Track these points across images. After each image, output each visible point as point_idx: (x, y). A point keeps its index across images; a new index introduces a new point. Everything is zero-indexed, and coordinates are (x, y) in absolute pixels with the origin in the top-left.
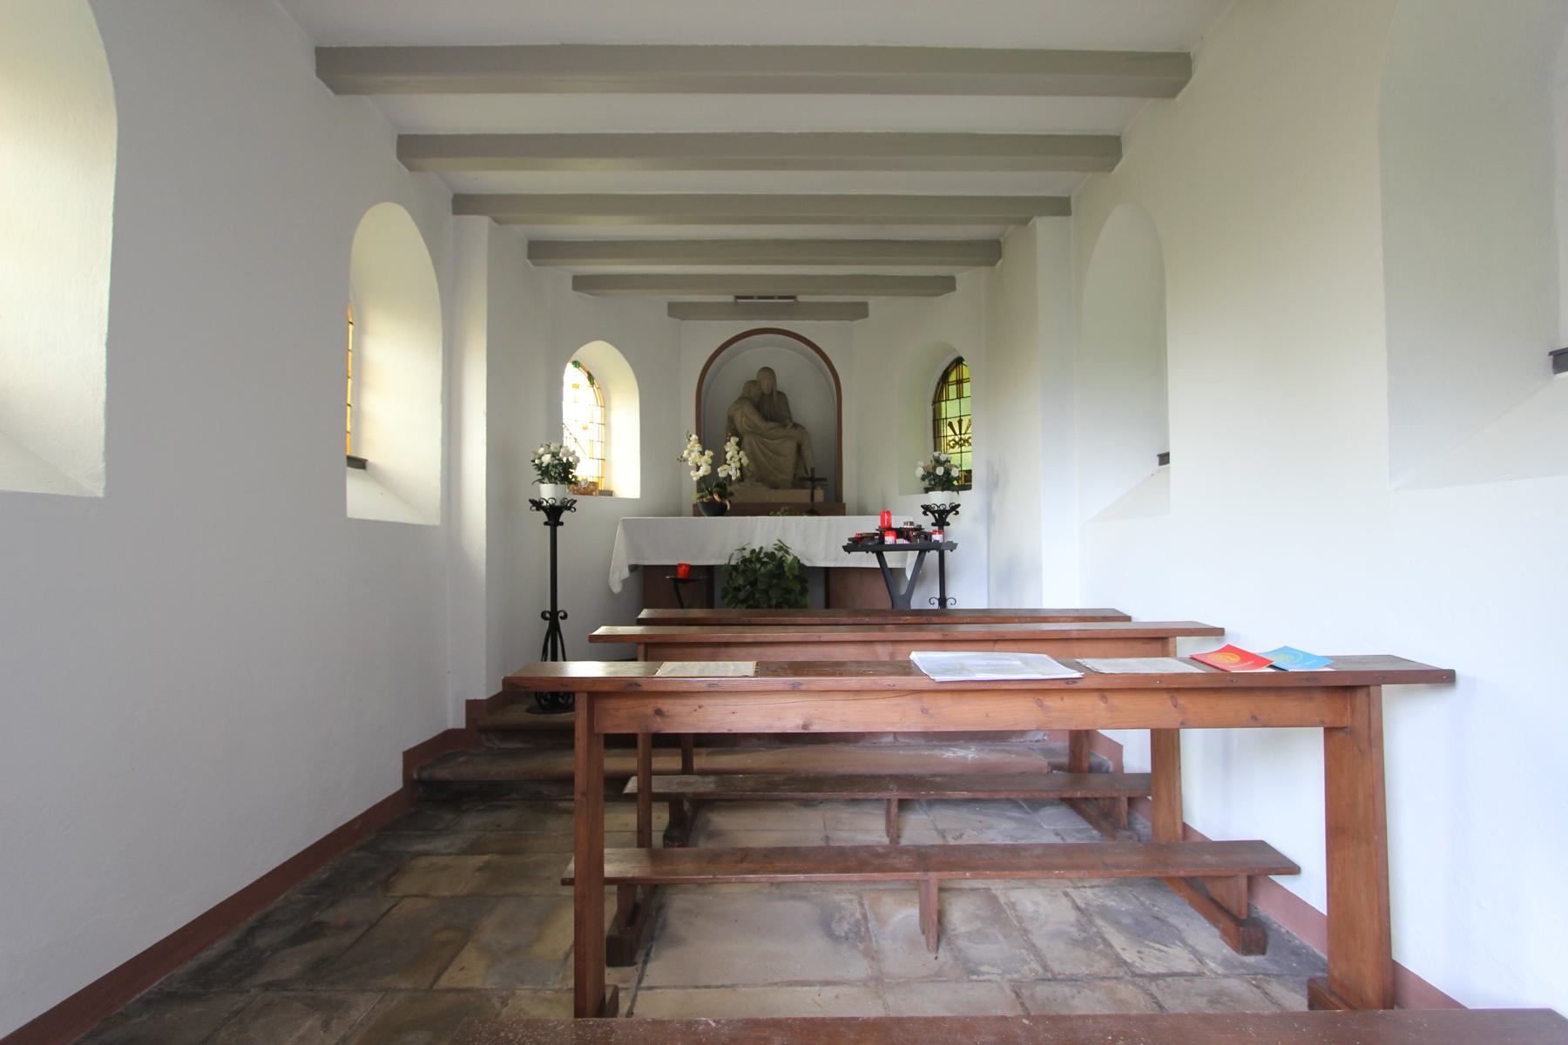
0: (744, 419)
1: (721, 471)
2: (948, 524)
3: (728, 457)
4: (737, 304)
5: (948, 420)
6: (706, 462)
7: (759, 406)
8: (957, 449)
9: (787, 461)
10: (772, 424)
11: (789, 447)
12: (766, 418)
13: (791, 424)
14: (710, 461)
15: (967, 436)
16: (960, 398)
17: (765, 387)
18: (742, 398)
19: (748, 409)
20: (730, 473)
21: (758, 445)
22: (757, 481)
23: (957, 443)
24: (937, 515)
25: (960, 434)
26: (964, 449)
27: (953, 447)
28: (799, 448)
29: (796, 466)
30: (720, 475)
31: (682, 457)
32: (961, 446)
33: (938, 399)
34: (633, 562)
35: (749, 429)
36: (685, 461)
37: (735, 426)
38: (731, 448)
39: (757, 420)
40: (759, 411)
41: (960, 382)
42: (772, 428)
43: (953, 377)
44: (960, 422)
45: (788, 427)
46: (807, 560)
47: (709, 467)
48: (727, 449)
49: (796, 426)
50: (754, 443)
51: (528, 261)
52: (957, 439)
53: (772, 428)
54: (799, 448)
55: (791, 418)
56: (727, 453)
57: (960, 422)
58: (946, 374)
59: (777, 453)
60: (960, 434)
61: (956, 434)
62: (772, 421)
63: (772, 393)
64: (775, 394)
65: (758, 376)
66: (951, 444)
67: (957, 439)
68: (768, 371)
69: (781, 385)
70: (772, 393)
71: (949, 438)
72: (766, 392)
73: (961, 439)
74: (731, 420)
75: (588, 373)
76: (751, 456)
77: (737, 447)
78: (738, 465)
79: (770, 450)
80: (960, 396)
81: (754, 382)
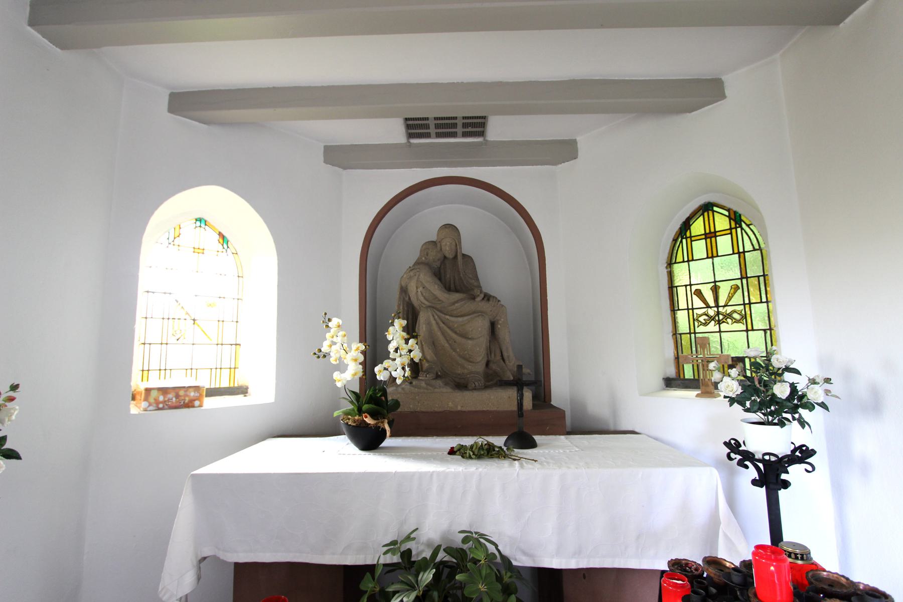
0: (420, 289)
1: (380, 371)
2: (786, 484)
3: (391, 347)
4: (410, 145)
5: (694, 288)
6: (355, 360)
7: (438, 274)
8: (712, 327)
9: (478, 347)
10: (456, 296)
11: (479, 327)
12: (449, 288)
13: (482, 296)
14: (361, 358)
15: (729, 310)
16: (712, 257)
17: (448, 251)
18: (418, 263)
19: (426, 277)
20: (394, 374)
21: (437, 323)
22: (437, 377)
23: (711, 318)
24: (761, 465)
25: (717, 306)
26: (724, 327)
27: (706, 324)
28: (493, 325)
29: (490, 351)
30: (378, 377)
31: (320, 351)
32: (719, 322)
33: (670, 264)
34: (207, 552)
35: (426, 303)
36: (324, 356)
37: (410, 299)
38: (395, 334)
39: (436, 290)
40: (440, 279)
41: (711, 235)
42: (457, 302)
43: (698, 227)
44: (715, 290)
45: (478, 299)
46: (525, 553)
47: (361, 366)
48: (389, 337)
49: (487, 297)
50: (433, 322)
51: (29, 29)
52: (711, 312)
53: (457, 302)
54: (493, 325)
55: (479, 287)
56: (389, 342)
57: (715, 290)
58: (686, 225)
59: (464, 336)
60: (717, 306)
61: (708, 307)
62: (457, 291)
63: (456, 257)
64: (460, 257)
65: (438, 235)
66: (702, 319)
67: (711, 312)
68: (450, 229)
69: (466, 249)
70: (456, 257)
71: (700, 312)
72: (447, 255)
73: (718, 313)
74: (404, 290)
75: (220, 234)
76: (431, 343)
77: (404, 334)
78: (406, 361)
79: (456, 333)
80: (712, 255)
81: (434, 243)
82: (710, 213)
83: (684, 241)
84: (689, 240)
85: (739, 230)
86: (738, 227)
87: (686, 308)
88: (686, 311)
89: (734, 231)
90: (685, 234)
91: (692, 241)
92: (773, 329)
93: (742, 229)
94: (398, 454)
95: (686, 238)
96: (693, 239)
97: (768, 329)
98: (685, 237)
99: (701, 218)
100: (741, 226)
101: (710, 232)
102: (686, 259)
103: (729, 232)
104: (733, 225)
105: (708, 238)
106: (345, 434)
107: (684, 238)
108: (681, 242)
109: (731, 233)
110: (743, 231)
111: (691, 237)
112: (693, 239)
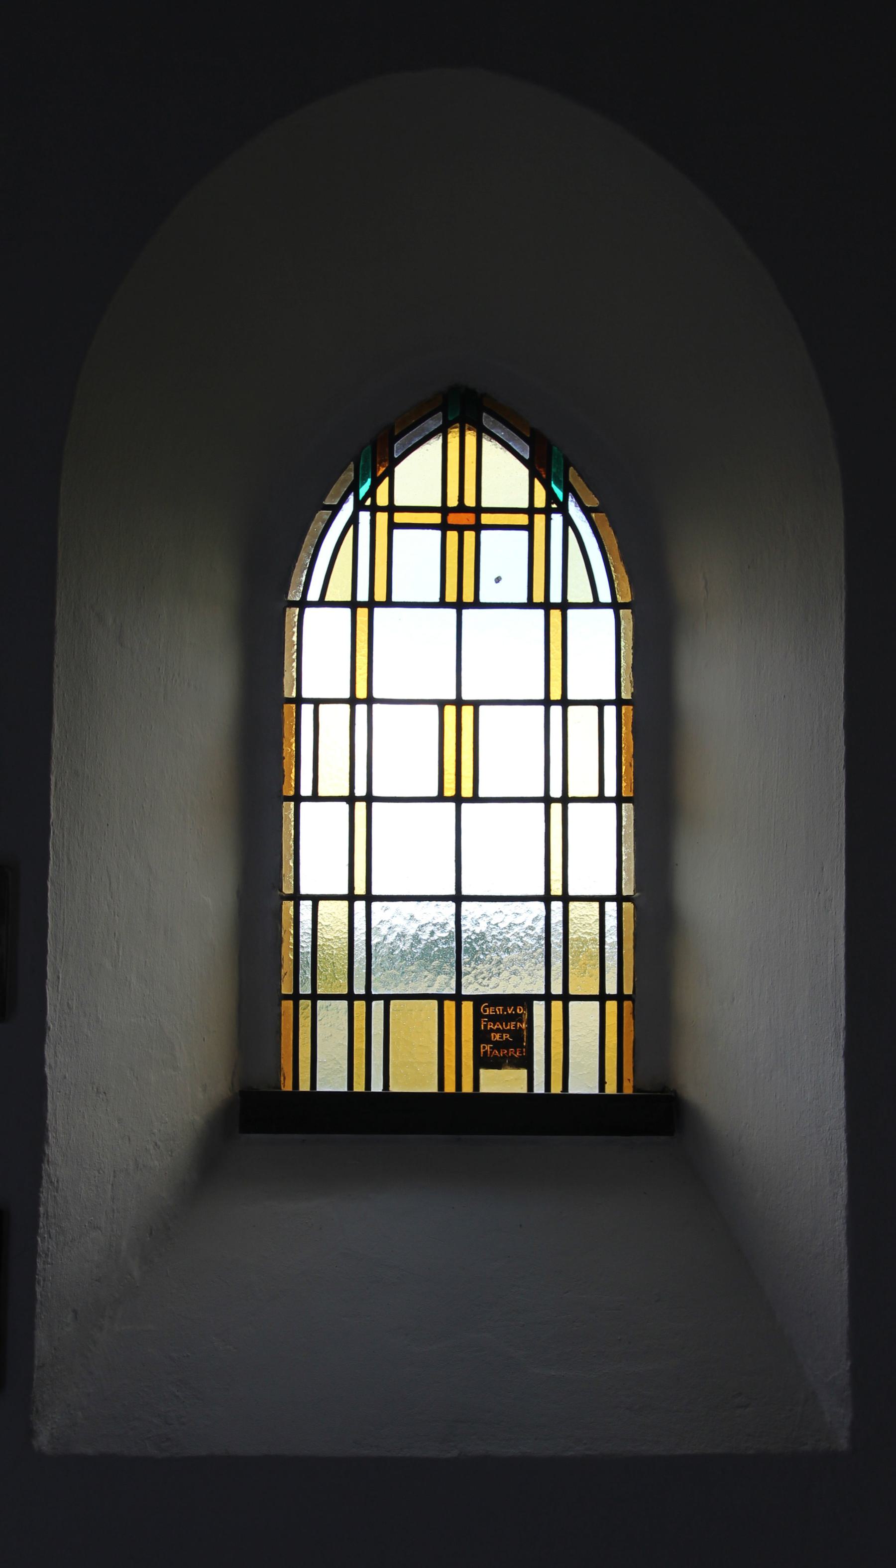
82: (471, 438)
83: (364, 517)
84: (382, 518)
85: (557, 520)
86: (556, 511)
87: (375, 805)
88: (375, 891)
89: (539, 520)
90: (372, 493)
91: (392, 526)
92: (481, 930)
93: (568, 522)
94: (282, 1082)
95: (374, 509)
96: (399, 518)
97: (609, 702)
98: (368, 502)
99: (436, 444)
100: (563, 509)
101: (461, 508)
102: (378, 1007)
103: (523, 519)
104: (540, 501)
105: (453, 528)
106: (383, 1090)
107: (366, 509)
108: (354, 521)
109: (529, 528)
110: (570, 530)
111: (391, 509)
112: (399, 518)
